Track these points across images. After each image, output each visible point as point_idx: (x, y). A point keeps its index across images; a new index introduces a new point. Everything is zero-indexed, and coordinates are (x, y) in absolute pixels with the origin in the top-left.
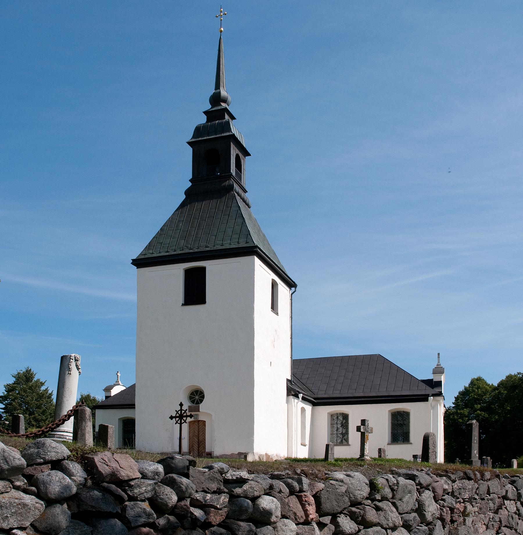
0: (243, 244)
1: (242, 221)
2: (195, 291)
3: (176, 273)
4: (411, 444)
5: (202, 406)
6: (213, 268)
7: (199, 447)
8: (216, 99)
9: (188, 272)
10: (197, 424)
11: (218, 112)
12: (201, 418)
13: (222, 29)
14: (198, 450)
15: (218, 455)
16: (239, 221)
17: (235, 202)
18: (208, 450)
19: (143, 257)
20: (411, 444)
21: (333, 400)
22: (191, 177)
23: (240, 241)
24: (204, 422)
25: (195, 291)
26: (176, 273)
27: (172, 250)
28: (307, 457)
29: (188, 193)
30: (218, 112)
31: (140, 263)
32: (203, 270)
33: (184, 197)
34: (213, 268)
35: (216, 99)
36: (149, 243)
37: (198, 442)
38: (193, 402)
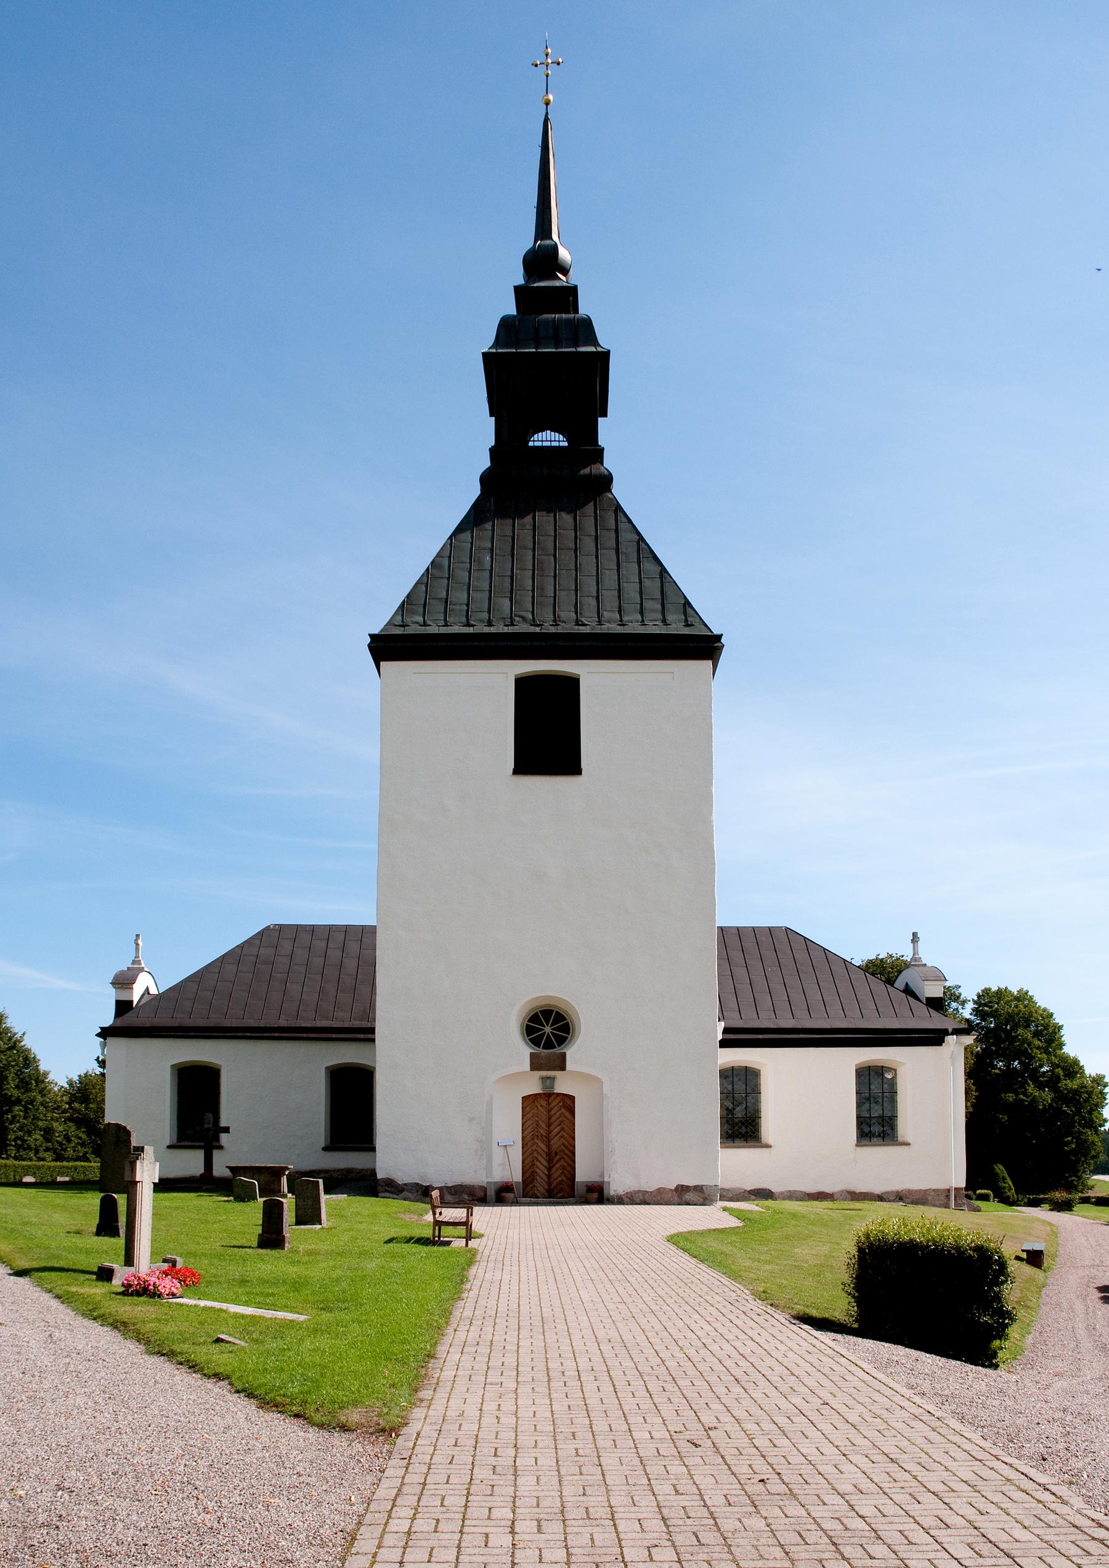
0: (676, 627)
1: (659, 569)
2: (547, 737)
3: (494, 684)
4: (768, 1146)
5: (575, 1053)
6: (600, 683)
7: (549, 1169)
8: (542, 261)
9: (523, 684)
10: (544, 1103)
11: (545, 295)
12: (563, 1086)
13: (551, 97)
14: (549, 1176)
15: (621, 1192)
16: (648, 566)
17: (624, 519)
18: (583, 1174)
19: (399, 631)
20: (768, 1146)
21: (330, 1035)
22: (492, 442)
23: (670, 618)
24: (572, 1099)
25: (547, 737)
26: (494, 684)
27: (482, 621)
28: (577, 1180)
29: (486, 479)
30: (545, 295)
31: (386, 648)
32: (572, 684)
33: (475, 491)
34: (600, 683)
35: (542, 261)
36: (408, 596)
37: (548, 1154)
38: (535, 1042)
